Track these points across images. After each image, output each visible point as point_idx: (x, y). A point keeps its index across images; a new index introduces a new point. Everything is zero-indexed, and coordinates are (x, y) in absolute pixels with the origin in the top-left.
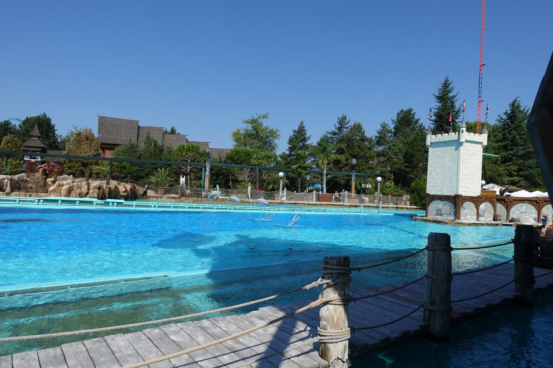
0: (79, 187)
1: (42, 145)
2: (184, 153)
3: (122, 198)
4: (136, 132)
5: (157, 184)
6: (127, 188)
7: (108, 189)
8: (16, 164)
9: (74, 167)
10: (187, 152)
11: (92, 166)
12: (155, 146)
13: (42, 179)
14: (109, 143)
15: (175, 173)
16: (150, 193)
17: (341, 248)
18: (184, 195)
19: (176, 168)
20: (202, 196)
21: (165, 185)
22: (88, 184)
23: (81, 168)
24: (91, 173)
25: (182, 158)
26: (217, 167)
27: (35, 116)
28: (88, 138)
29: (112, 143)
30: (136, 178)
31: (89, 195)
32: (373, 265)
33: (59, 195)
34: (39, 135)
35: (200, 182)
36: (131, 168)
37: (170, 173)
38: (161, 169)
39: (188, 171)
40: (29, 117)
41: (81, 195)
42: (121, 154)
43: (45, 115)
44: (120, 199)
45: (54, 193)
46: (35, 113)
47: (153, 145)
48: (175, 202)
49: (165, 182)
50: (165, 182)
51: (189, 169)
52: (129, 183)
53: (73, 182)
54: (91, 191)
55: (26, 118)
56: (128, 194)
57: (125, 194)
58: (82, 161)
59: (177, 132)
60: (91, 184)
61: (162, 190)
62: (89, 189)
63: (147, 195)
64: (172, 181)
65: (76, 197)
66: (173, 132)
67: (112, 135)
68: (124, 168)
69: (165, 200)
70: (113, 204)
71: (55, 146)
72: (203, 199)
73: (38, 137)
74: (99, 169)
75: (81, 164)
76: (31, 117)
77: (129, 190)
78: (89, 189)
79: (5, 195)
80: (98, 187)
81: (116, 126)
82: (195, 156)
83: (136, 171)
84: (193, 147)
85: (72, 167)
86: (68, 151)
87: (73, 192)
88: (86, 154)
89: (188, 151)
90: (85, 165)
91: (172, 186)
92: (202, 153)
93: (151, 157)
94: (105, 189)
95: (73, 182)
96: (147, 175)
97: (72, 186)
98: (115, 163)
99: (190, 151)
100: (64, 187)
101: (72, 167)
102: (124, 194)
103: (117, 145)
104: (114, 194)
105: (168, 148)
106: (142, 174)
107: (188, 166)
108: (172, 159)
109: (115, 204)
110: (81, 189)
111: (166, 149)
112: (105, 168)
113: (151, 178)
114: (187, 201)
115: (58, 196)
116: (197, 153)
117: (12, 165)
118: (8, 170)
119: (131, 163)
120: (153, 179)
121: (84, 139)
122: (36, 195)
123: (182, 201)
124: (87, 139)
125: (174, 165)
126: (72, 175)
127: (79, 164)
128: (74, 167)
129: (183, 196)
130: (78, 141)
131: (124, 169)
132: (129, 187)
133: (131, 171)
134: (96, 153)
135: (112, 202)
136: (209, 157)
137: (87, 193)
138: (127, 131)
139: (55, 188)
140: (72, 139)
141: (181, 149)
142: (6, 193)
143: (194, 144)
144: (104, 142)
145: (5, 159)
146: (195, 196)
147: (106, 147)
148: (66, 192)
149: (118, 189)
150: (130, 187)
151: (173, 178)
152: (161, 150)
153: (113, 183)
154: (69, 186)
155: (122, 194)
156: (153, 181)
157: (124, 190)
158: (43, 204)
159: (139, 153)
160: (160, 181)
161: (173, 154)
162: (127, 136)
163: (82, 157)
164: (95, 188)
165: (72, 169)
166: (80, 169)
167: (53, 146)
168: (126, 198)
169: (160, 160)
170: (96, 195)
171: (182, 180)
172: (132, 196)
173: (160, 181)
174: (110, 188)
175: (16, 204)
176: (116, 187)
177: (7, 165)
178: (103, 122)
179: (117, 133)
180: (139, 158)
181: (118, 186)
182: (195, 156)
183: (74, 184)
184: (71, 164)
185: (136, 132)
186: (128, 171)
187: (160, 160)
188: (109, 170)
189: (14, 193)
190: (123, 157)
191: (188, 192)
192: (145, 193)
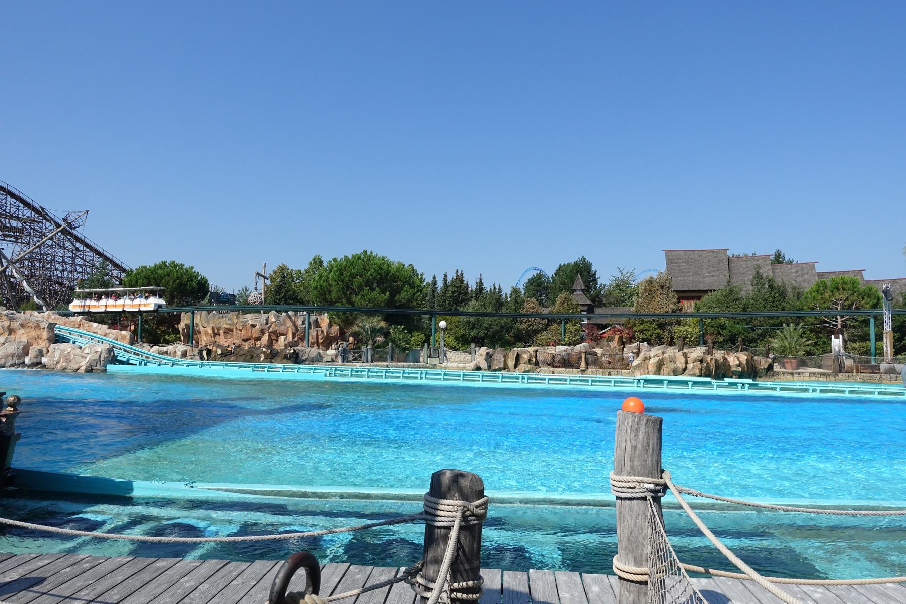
0: (673, 360)
1: (589, 302)
2: (827, 296)
3: (734, 376)
4: (725, 268)
5: (783, 351)
6: (741, 360)
7: (713, 361)
8: (575, 331)
9: (648, 330)
10: (832, 292)
11: (673, 327)
12: (771, 287)
13: (619, 350)
14: (687, 289)
15: (811, 331)
16: (777, 368)
17: (200, 499)
18: (843, 370)
19: (816, 322)
20: (881, 371)
21: (797, 352)
22: (685, 355)
23: (658, 331)
24: (672, 338)
25: (824, 303)
26: (899, 315)
27: (572, 261)
28: (664, 286)
29: (692, 289)
30: (748, 344)
31: (687, 372)
32: (192, 595)
33: (647, 372)
34: (583, 288)
35: (864, 345)
36: (735, 328)
37: (804, 332)
38: (788, 325)
39: (839, 326)
40: (562, 265)
41: (675, 372)
42: (714, 306)
43: (585, 259)
44: (732, 377)
45: (640, 370)
46: (571, 258)
47: (767, 286)
48: (827, 381)
49: (798, 347)
50: (798, 347)
51: (839, 322)
52: (741, 351)
53: (663, 353)
54: (690, 366)
55: (558, 266)
56: (743, 369)
57: (740, 369)
58: (658, 321)
59: (787, 259)
60: (688, 356)
61: (794, 361)
62: (686, 363)
63: (774, 370)
64: (808, 345)
65: (669, 374)
66: (778, 259)
67: (689, 277)
68: (723, 327)
69: (807, 378)
70: (717, 388)
71: (599, 301)
72: (884, 376)
73: (583, 290)
74: (683, 331)
75: (657, 325)
76: (564, 265)
77: (744, 362)
78: (686, 363)
79: (580, 373)
80: (700, 359)
81: (694, 262)
82: (851, 298)
83: (743, 331)
84: (844, 283)
85: (646, 330)
86: (637, 307)
87: (664, 368)
88: (662, 310)
89: (835, 290)
90: (662, 326)
91: (809, 354)
92: (864, 292)
93: (765, 307)
94: (709, 361)
95: (663, 353)
96: (763, 336)
97: (663, 358)
98: (708, 321)
99: (838, 289)
100: (652, 361)
101: (646, 330)
102: (737, 370)
103: (706, 292)
104: (721, 371)
105: (794, 288)
106: (753, 335)
107: (838, 316)
108: (805, 307)
109: (747, 386)
110: (675, 362)
111: (790, 290)
112: (691, 328)
113: (770, 342)
114: (851, 379)
115: (645, 374)
116: (855, 292)
117: (571, 332)
118: (567, 339)
119: (733, 318)
120: (775, 343)
121: (657, 288)
122: (616, 373)
123: (841, 381)
124: (662, 287)
125: (811, 317)
126: (645, 343)
127: (654, 325)
128: (648, 330)
129: (840, 372)
130: (651, 291)
131: (722, 329)
132: (743, 357)
133: (735, 331)
134: (676, 307)
135: (741, 383)
136: (890, 299)
137: (685, 369)
138: (711, 268)
139: (640, 362)
140: (641, 289)
141: (822, 288)
142: (581, 370)
143: (847, 278)
144: (679, 290)
145: (562, 325)
146: (866, 371)
147: (685, 295)
148: (655, 368)
149: (728, 361)
150: (746, 358)
151: (810, 339)
152: (783, 295)
153: (718, 355)
154: (658, 358)
155: (734, 369)
156: (776, 346)
157: (738, 363)
158: (592, 385)
159: (743, 302)
160: (788, 346)
161: (806, 298)
162: (713, 276)
163: (658, 315)
164: (695, 361)
165: (645, 334)
166: (657, 333)
167: (597, 301)
168: (741, 375)
169: (783, 309)
170: (697, 372)
171: (836, 343)
172: (751, 372)
173: (788, 346)
174: (716, 360)
175: (566, 384)
176: (725, 359)
177: (565, 331)
178: (672, 257)
179: (696, 273)
180: (744, 309)
181: (726, 356)
182: (851, 298)
183: (665, 355)
184: (643, 326)
185: (725, 268)
186: (730, 331)
187: (783, 309)
188: (700, 332)
189: (590, 370)
190: (718, 310)
191: (848, 363)
192: (770, 367)
